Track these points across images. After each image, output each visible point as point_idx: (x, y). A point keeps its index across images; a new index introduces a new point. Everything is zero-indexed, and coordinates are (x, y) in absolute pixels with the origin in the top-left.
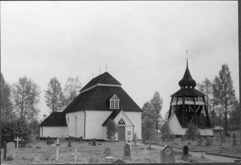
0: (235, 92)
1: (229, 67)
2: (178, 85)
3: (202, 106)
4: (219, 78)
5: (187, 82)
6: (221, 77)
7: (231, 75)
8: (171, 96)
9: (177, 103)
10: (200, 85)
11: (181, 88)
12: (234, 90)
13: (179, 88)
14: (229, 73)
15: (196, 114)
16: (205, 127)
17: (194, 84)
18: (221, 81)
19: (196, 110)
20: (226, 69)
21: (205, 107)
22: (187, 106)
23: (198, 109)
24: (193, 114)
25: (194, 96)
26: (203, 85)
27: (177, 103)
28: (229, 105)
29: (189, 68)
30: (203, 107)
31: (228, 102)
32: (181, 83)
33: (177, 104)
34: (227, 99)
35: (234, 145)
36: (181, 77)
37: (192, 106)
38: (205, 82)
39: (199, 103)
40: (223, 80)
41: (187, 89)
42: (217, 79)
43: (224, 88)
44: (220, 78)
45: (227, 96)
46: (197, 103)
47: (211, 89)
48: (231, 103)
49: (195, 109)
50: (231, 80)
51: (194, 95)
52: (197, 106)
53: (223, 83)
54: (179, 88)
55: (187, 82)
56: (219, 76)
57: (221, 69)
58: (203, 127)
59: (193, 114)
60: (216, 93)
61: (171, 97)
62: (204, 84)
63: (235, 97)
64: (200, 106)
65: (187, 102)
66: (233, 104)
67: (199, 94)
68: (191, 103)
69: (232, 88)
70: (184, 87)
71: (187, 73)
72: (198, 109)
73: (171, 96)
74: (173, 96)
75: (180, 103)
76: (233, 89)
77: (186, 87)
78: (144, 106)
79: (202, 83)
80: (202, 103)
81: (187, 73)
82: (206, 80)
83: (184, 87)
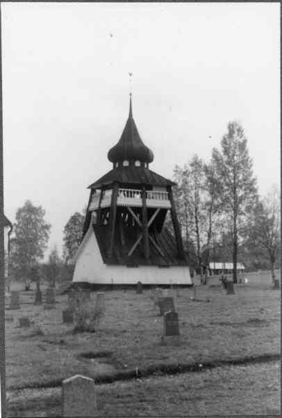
0: (258, 184)
1: (244, 127)
2: (107, 160)
3: (163, 211)
4: (222, 153)
5: (130, 155)
6: (226, 151)
7: (248, 146)
8: (88, 188)
9: (100, 203)
10: (179, 170)
11: (114, 166)
12: (254, 180)
13: (108, 167)
14: (245, 141)
15: (147, 230)
16: (170, 263)
17: (146, 156)
18: (225, 158)
19: (149, 219)
20: (236, 132)
21: (172, 213)
22: (123, 209)
23: (153, 218)
24: (141, 230)
25: (144, 184)
26: (187, 171)
27: (100, 203)
28: (242, 213)
29: (134, 117)
30: (169, 211)
31: (242, 207)
32: (115, 155)
33: (100, 207)
34: (238, 201)
35: (167, 338)
36: (114, 138)
37: (137, 210)
38: (192, 165)
39: (157, 201)
40: (229, 157)
41: (126, 167)
42: (216, 157)
43: (231, 174)
44: (225, 154)
45: (240, 193)
46: (150, 203)
47: (203, 180)
48: (248, 209)
49: (145, 219)
50: (249, 157)
51: (149, 183)
52: (151, 211)
53: (229, 163)
54: (108, 167)
55: (130, 155)
56: (220, 149)
57: (226, 131)
58: (163, 262)
59: (141, 230)
60: (215, 187)
61: (90, 190)
62: (190, 169)
63: (256, 194)
64: (158, 211)
65: (123, 200)
66: (252, 212)
67: (158, 181)
68: (136, 200)
69: (250, 174)
70: (121, 164)
71: (130, 130)
72: (153, 218)
73: (88, 188)
74: (93, 188)
75: (106, 203)
76: (252, 177)
77: (126, 163)
78: (70, 221)
79: (185, 167)
80: (166, 204)
81: (130, 130)
82: (194, 161)
83: (119, 165)
